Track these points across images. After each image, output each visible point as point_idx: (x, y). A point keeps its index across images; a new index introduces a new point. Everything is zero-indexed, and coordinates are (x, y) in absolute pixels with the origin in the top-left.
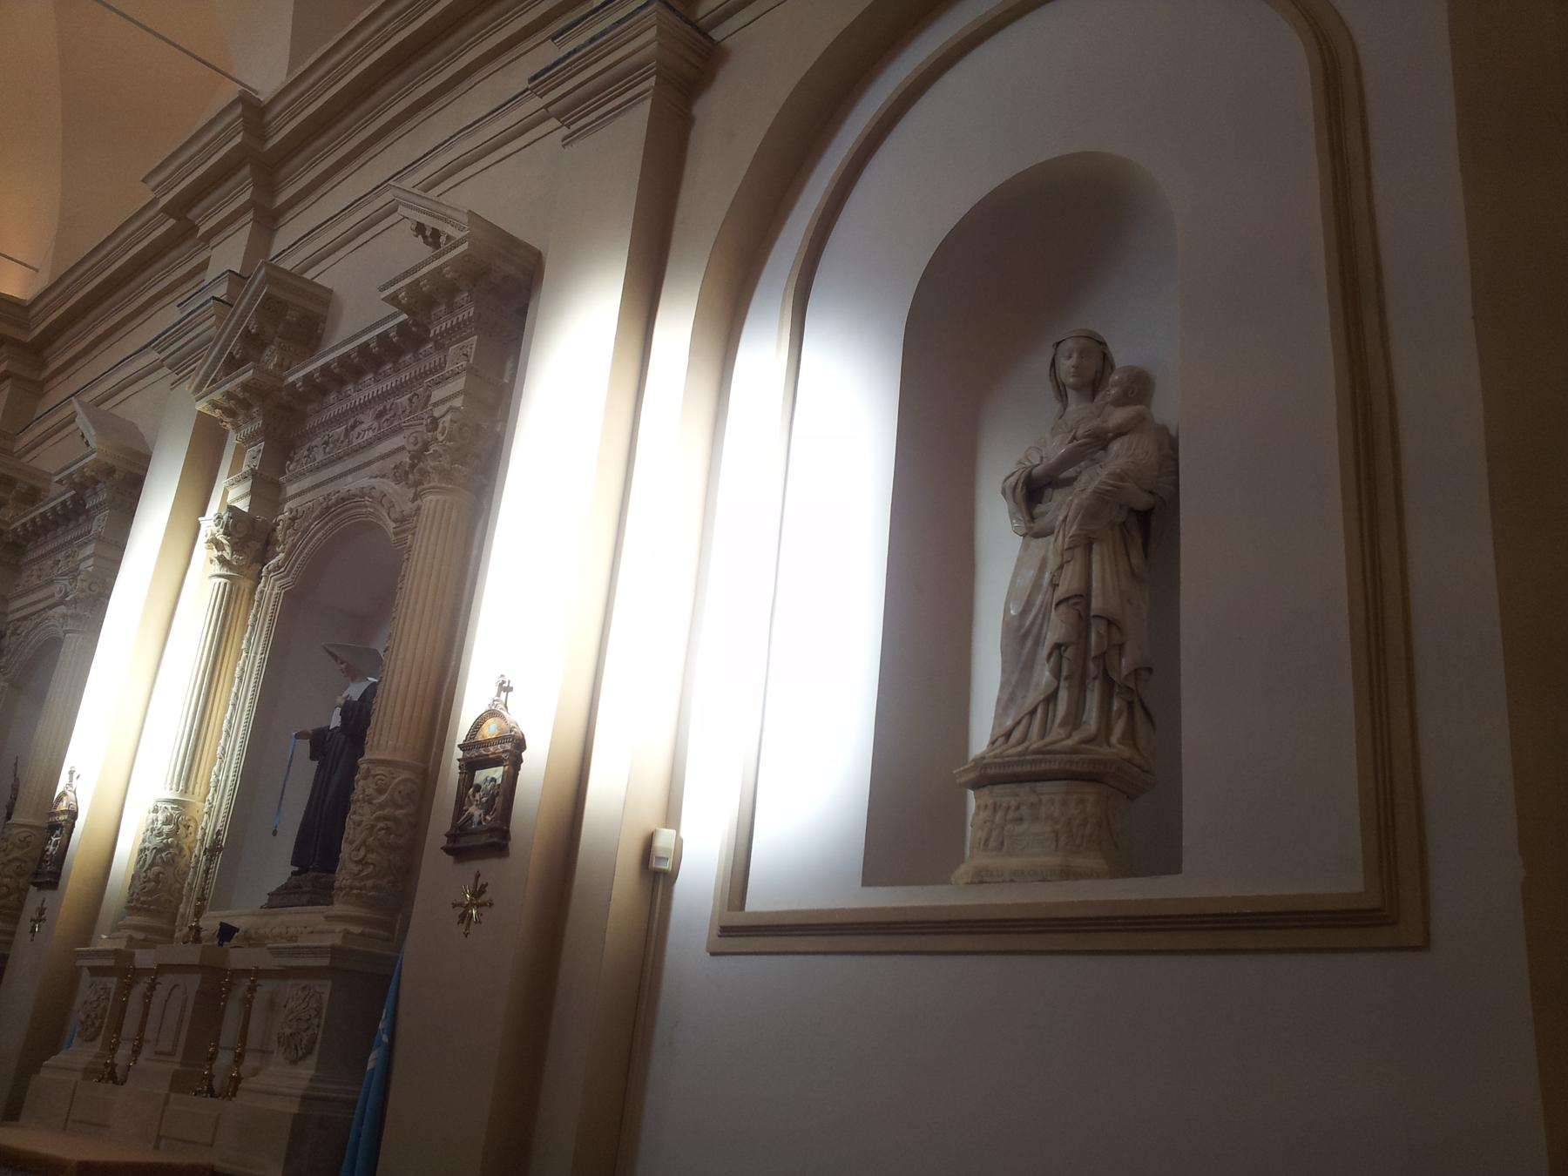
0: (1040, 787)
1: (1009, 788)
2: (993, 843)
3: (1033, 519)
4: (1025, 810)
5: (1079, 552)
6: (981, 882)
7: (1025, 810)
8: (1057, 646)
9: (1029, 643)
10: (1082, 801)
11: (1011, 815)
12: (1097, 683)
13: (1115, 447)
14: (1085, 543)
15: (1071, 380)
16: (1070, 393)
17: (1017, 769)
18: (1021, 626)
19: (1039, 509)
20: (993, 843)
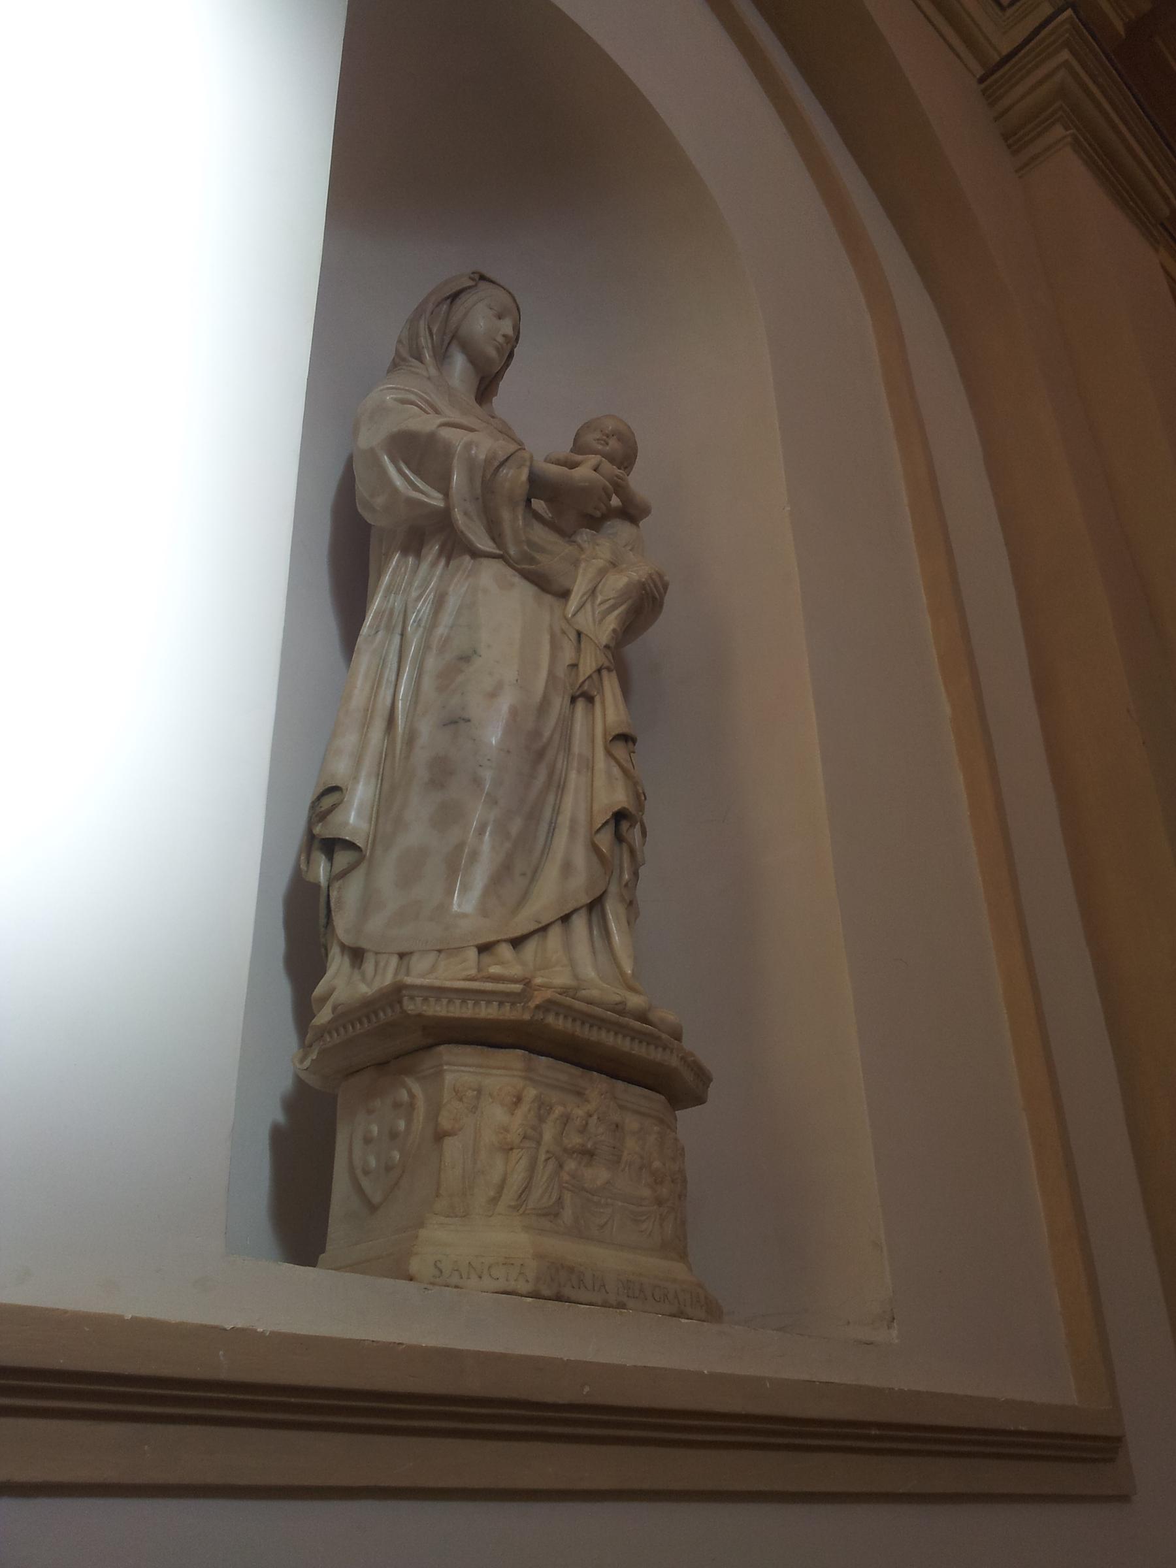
1: (564, 1073)
6: (558, 1298)
11: (575, 1140)
17: (608, 1039)
18: (536, 734)
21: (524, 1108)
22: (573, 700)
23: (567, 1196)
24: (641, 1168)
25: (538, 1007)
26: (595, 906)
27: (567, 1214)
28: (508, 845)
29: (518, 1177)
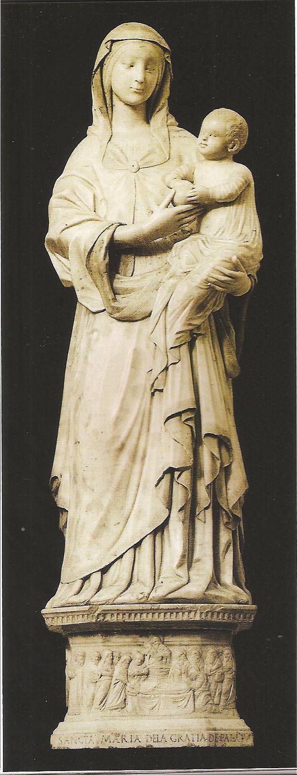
0: (168, 639)
2: (113, 699)
3: (115, 293)
4: (152, 664)
5: (185, 349)
7: (152, 664)
8: (171, 471)
9: (125, 458)
10: (218, 655)
11: (134, 669)
12: (209, 513)
13: (216, 218)
14: (190, 339)
15: (134, 98)
16: (119, 106)
17: (147, 618)
18: (115, 438)
19: (121, 282)
20: (113, 699)
21: (102, 661)
22: (153, 394)
23: (129, 700)
24: (181, 674)
25: (99, 614)
26: (160, 530)
27: (129, 707)
28: (102, 513)
29: (99, 696)
